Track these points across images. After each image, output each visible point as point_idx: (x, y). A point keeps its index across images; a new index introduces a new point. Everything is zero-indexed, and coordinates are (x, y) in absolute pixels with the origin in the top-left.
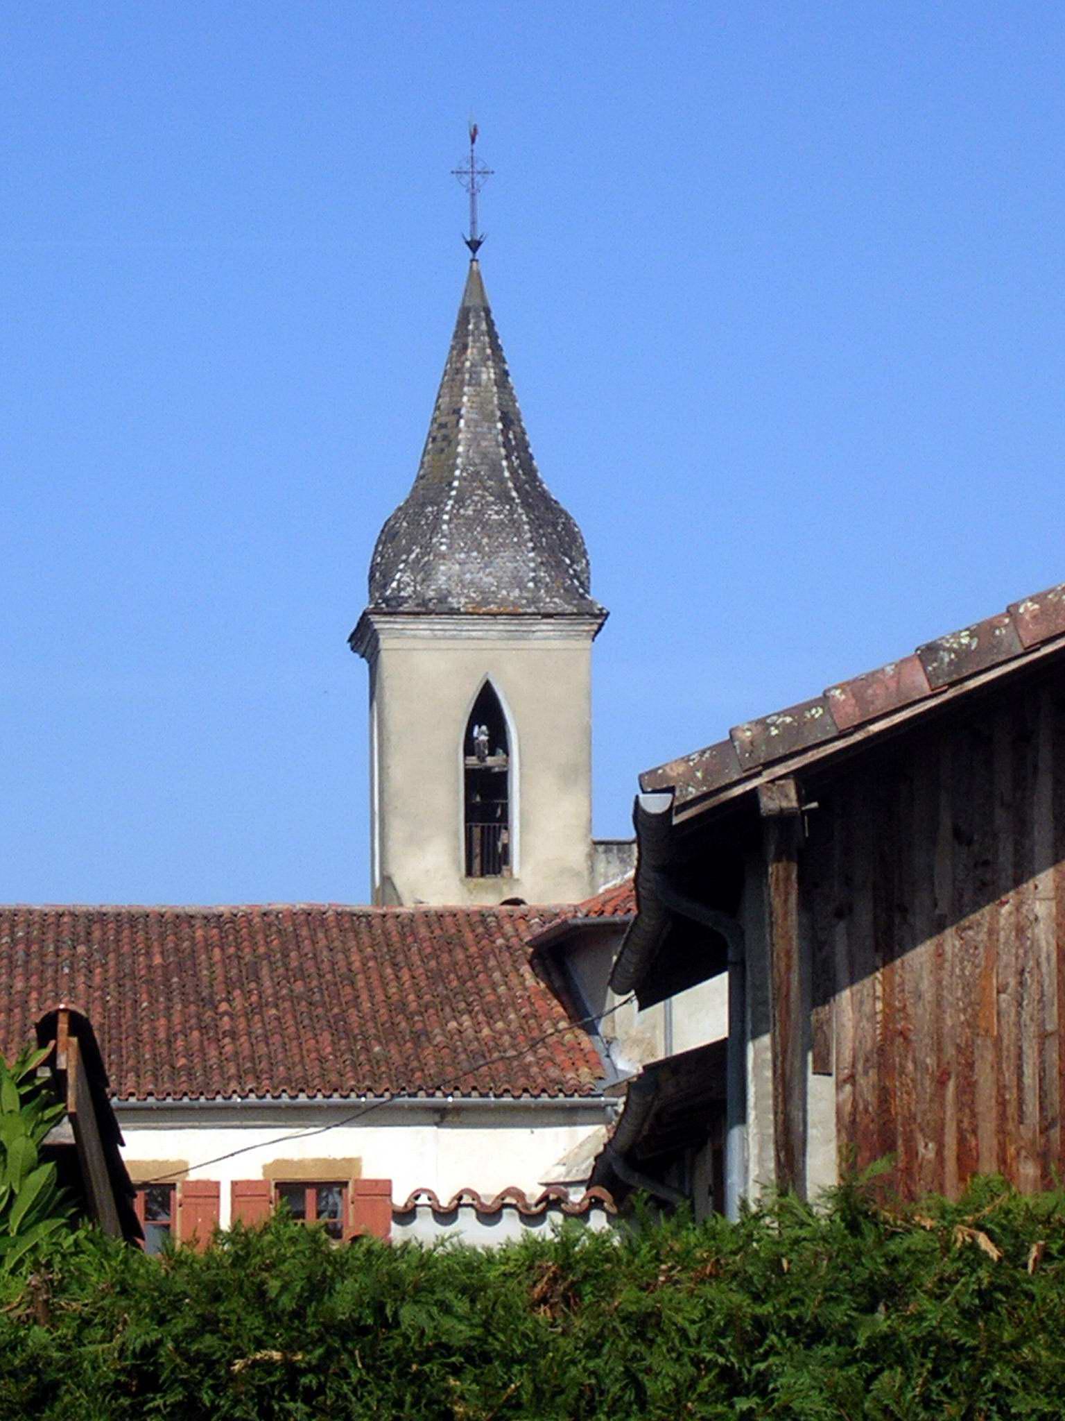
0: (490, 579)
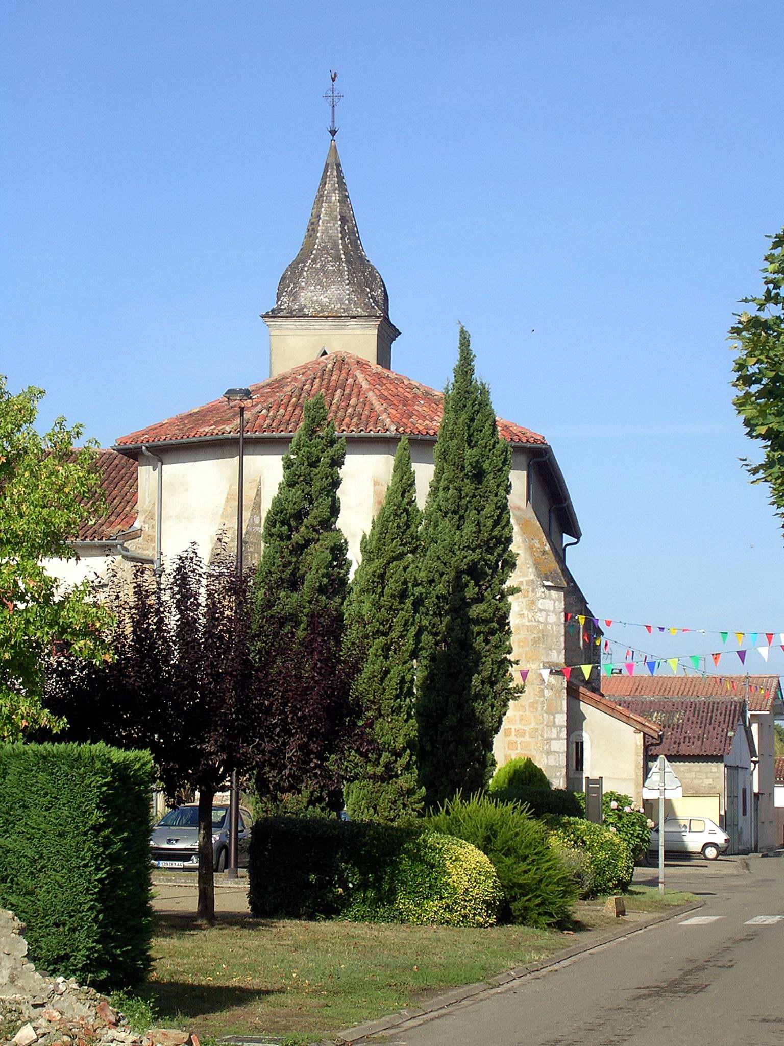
0: (327, 300)
